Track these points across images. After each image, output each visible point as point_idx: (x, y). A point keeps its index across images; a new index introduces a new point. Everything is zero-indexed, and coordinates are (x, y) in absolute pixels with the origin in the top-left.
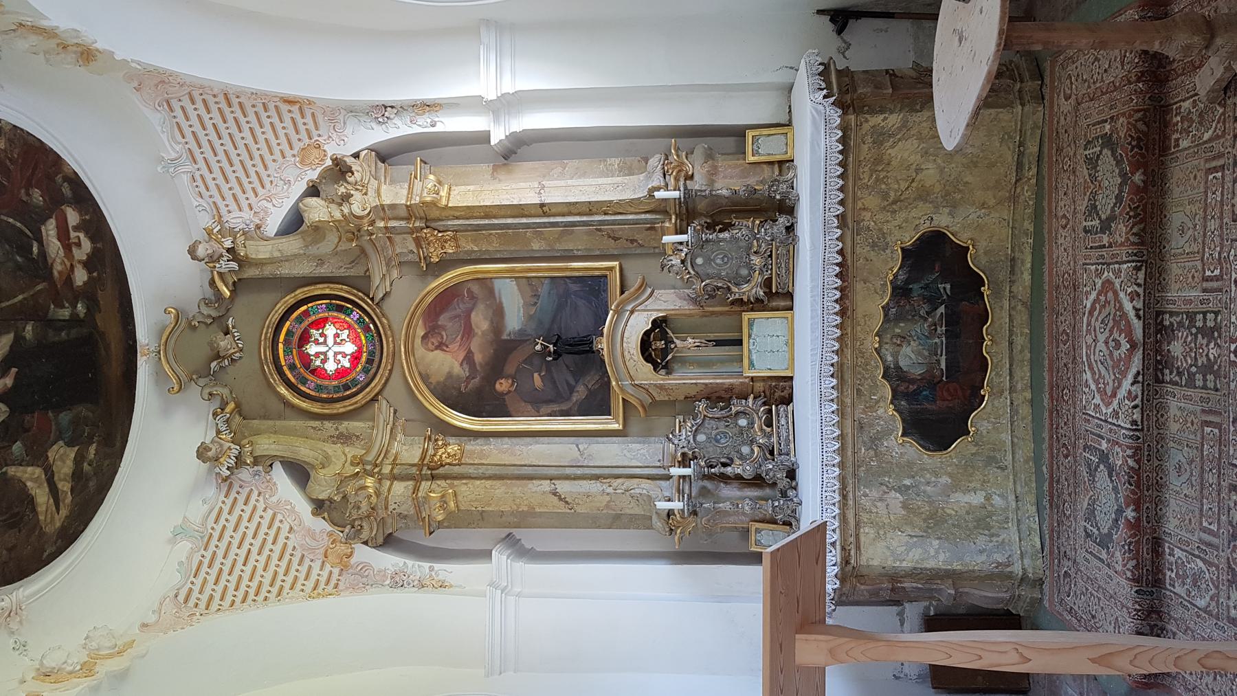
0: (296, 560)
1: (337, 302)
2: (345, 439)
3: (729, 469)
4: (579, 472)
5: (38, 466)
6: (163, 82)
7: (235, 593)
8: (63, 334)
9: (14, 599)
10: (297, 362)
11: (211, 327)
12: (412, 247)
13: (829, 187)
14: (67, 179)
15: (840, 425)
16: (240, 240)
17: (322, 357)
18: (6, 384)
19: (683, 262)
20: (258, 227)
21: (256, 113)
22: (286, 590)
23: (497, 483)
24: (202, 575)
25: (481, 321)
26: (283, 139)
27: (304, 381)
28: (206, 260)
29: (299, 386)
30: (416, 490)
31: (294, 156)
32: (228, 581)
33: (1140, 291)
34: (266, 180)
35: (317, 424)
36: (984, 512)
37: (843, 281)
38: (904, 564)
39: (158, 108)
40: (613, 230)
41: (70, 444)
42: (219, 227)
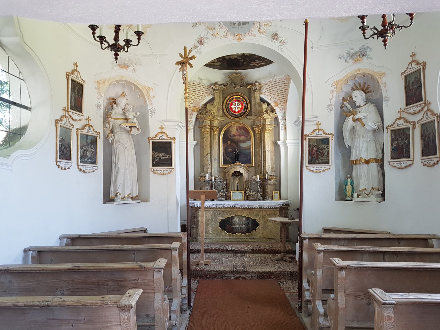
0: (194, 101)
2: (218, 110)
3: (214, 188)
4: (212, 158)
12: (257, 124)
13: (267, 205)
15: (224, 208)
16: (259, 91)
17: (235, 105)
19: (254, 179)
20: (262, 93)
21: (283, 101)
23: (210, 142)
24: (192, 84)
25: (242, 138)
26: (279, 99)
30: (208, 126)
31: (276, 100)
33: (248, 250)
34: (271, 95)
35: (221, 104)
36: (208, 233)
37: (250, 208)
38: (199, 219)
40: (260, 165)
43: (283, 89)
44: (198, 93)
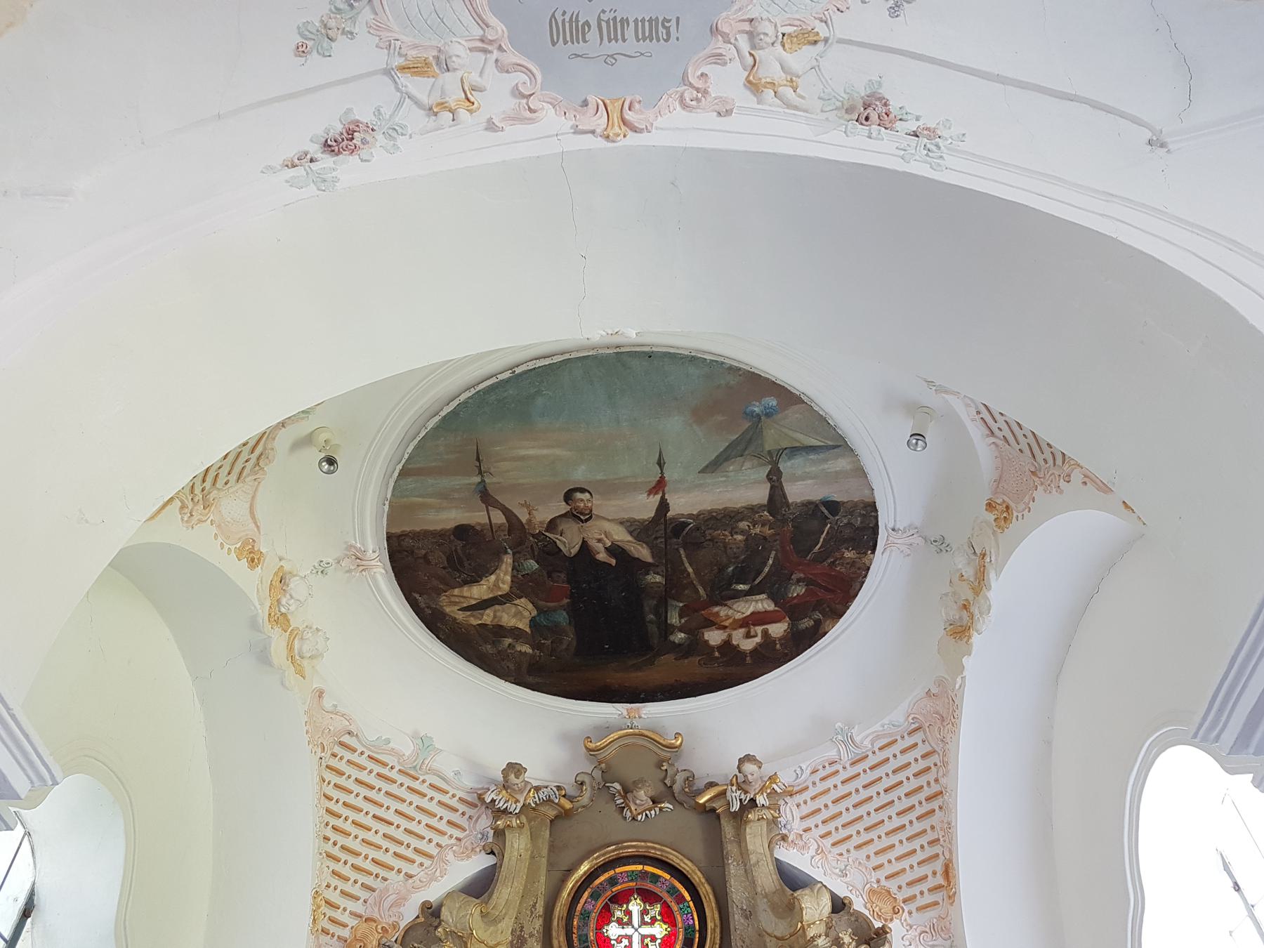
0: (369, 881)
1: (697, 940)
5: (511, 587)
6: (943, 719)
7: (341, 803)
8: (652, 616)
9: (373, 563)
10: (620, 887)
11: (661, 784)
14: (818, 623)
16: (767, 814)
18: (599, 553)
20: (784, 838)
21: (925, 831)
22: (334, 866)
24: (370, 765)
26: (897, 866)
27: (595, 896)
28: (741, 779)
29: (589, 890)
31: (878, 881)
32: (357, 795)
34: (842, 848)
35: (540, 909)
39: (910, 718)
41: (533, 622)
42: (779, 791)
43: (913, 800)
44: (399, 834)
